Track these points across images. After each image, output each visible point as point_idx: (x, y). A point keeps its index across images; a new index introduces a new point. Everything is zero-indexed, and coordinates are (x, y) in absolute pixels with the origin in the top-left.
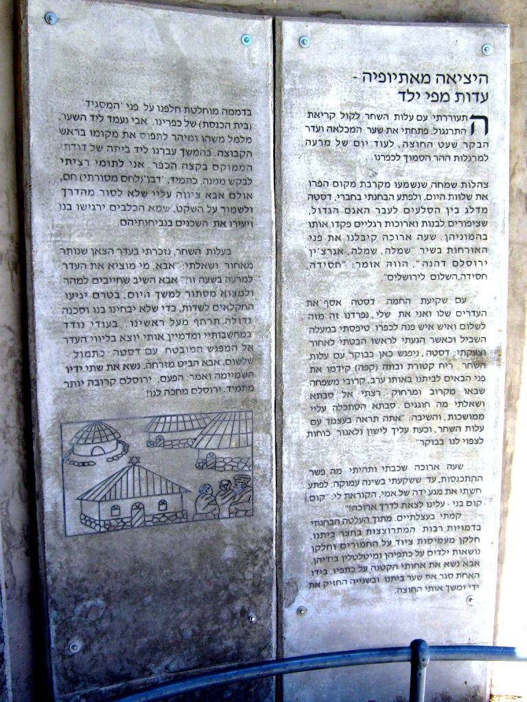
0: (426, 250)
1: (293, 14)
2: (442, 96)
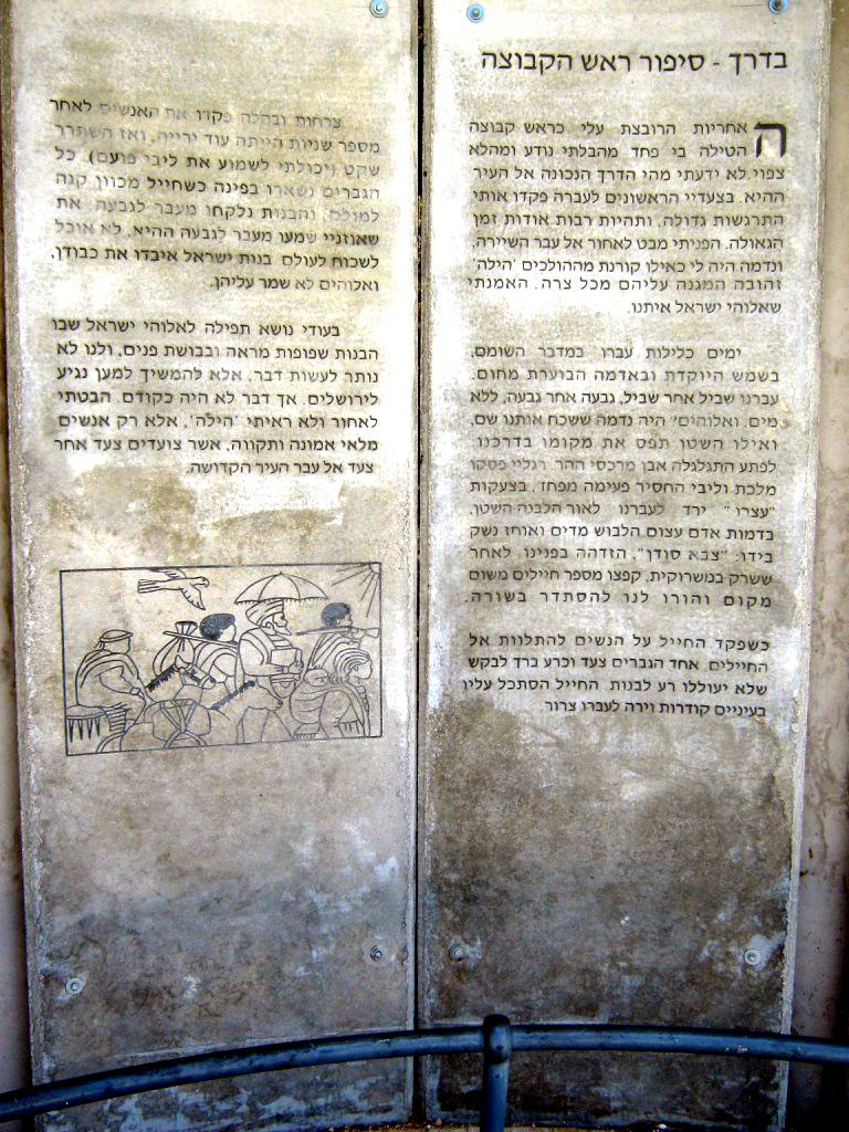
0: (646, 487)
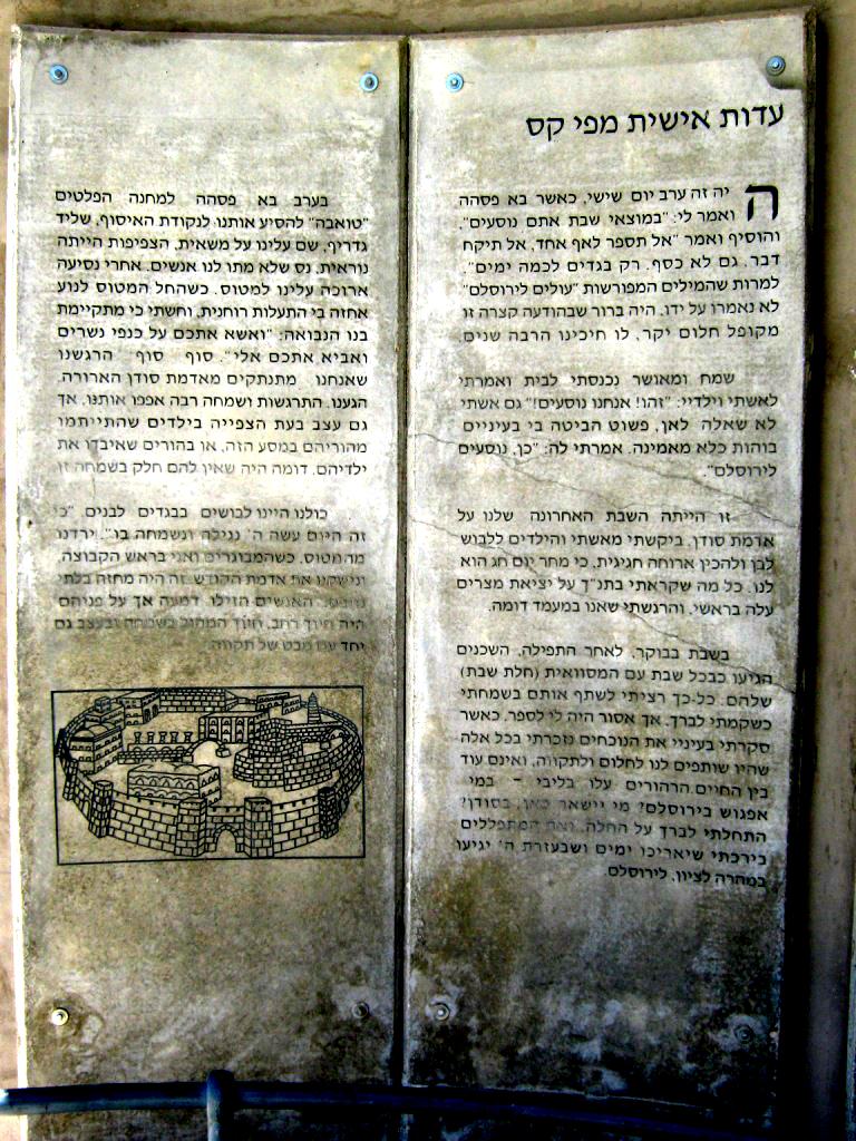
1: (422, 32)
2: (604, 122)
